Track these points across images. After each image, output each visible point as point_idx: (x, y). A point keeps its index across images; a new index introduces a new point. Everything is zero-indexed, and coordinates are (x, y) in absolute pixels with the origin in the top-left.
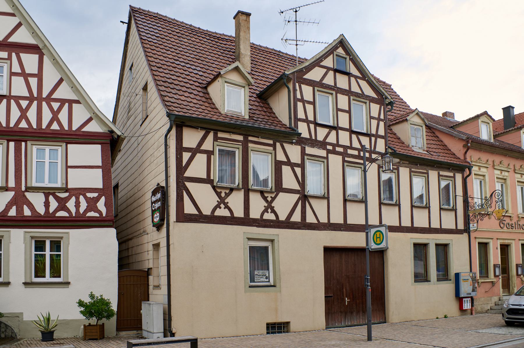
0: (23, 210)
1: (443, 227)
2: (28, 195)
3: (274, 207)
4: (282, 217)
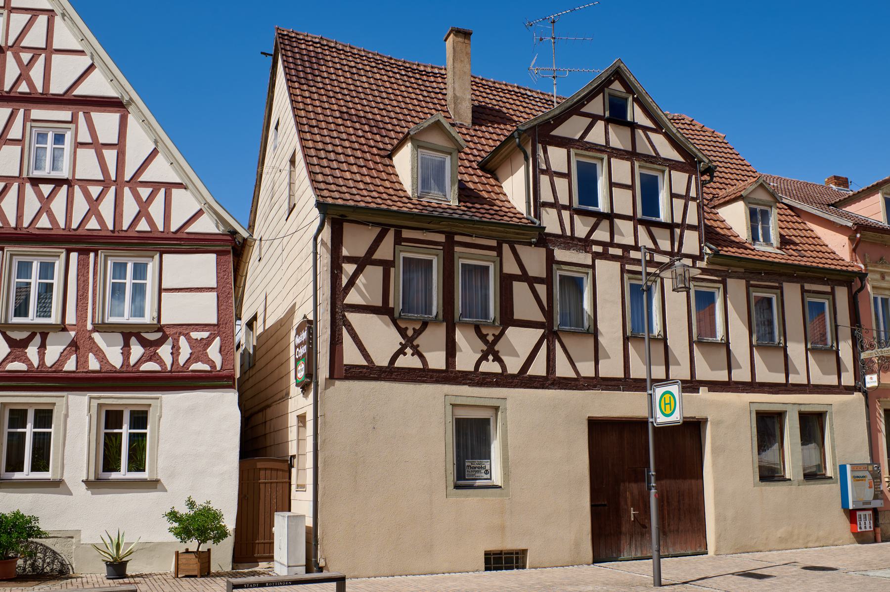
0: (86, 361)
2: (97, 336)
3: (498, 352)
4: (513, 366)
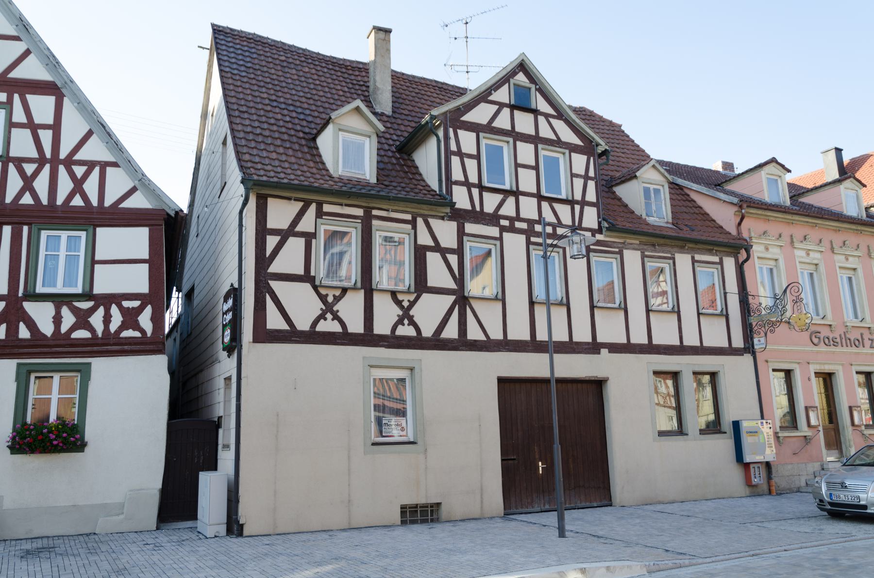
1: (706, 344)
2: (28, 306)
4: (428, 332)
